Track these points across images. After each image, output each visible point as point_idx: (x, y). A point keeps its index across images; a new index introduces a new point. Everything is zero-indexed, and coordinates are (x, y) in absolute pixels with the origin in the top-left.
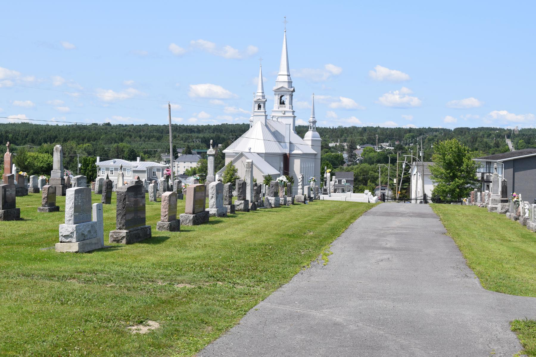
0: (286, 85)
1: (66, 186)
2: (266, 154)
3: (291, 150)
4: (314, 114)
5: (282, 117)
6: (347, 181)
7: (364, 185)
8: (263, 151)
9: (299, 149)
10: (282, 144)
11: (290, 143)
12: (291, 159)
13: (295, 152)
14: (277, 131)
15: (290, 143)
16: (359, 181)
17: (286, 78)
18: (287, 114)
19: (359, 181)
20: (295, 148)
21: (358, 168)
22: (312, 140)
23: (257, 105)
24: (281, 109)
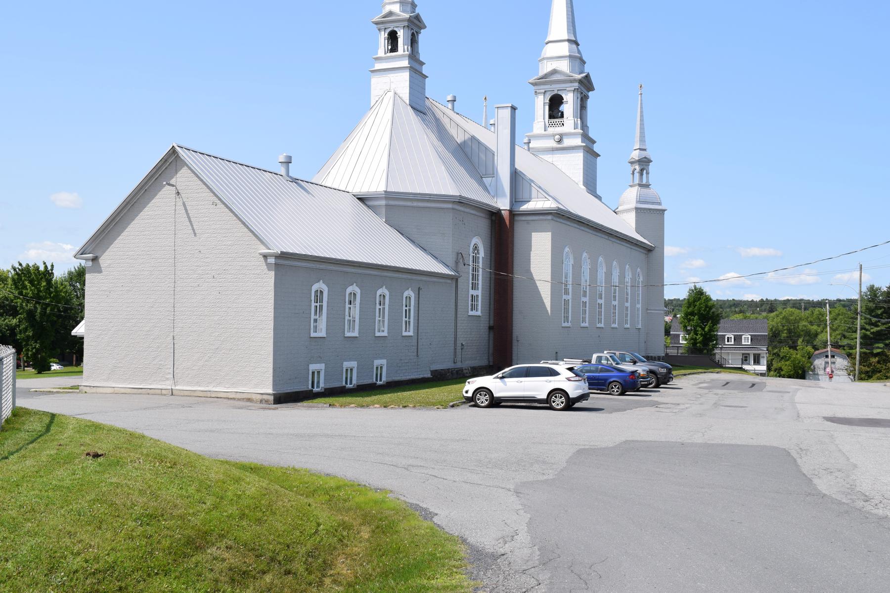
0: (564, 66)
1: (20, 331)
2: (389, 195)
3: (515, 199)
4: (642, 139)
5: (553, 150)
6: (753, 338)
7: (790, 347)
8: (376, 185)
9: (548, 195)
10: (487, 181)
11: (515, 175)
12: (520, 229)
13: (535, 204)
14: (473, 138)
15: (515, 175)
16: (781, 342)
17: (564, 49)
18: (567, 142)
19: (781, 342)
20: (534, 193)
21: (777, 316)
22: (637, 209)
23: (384, 35)
24: (551, 130)
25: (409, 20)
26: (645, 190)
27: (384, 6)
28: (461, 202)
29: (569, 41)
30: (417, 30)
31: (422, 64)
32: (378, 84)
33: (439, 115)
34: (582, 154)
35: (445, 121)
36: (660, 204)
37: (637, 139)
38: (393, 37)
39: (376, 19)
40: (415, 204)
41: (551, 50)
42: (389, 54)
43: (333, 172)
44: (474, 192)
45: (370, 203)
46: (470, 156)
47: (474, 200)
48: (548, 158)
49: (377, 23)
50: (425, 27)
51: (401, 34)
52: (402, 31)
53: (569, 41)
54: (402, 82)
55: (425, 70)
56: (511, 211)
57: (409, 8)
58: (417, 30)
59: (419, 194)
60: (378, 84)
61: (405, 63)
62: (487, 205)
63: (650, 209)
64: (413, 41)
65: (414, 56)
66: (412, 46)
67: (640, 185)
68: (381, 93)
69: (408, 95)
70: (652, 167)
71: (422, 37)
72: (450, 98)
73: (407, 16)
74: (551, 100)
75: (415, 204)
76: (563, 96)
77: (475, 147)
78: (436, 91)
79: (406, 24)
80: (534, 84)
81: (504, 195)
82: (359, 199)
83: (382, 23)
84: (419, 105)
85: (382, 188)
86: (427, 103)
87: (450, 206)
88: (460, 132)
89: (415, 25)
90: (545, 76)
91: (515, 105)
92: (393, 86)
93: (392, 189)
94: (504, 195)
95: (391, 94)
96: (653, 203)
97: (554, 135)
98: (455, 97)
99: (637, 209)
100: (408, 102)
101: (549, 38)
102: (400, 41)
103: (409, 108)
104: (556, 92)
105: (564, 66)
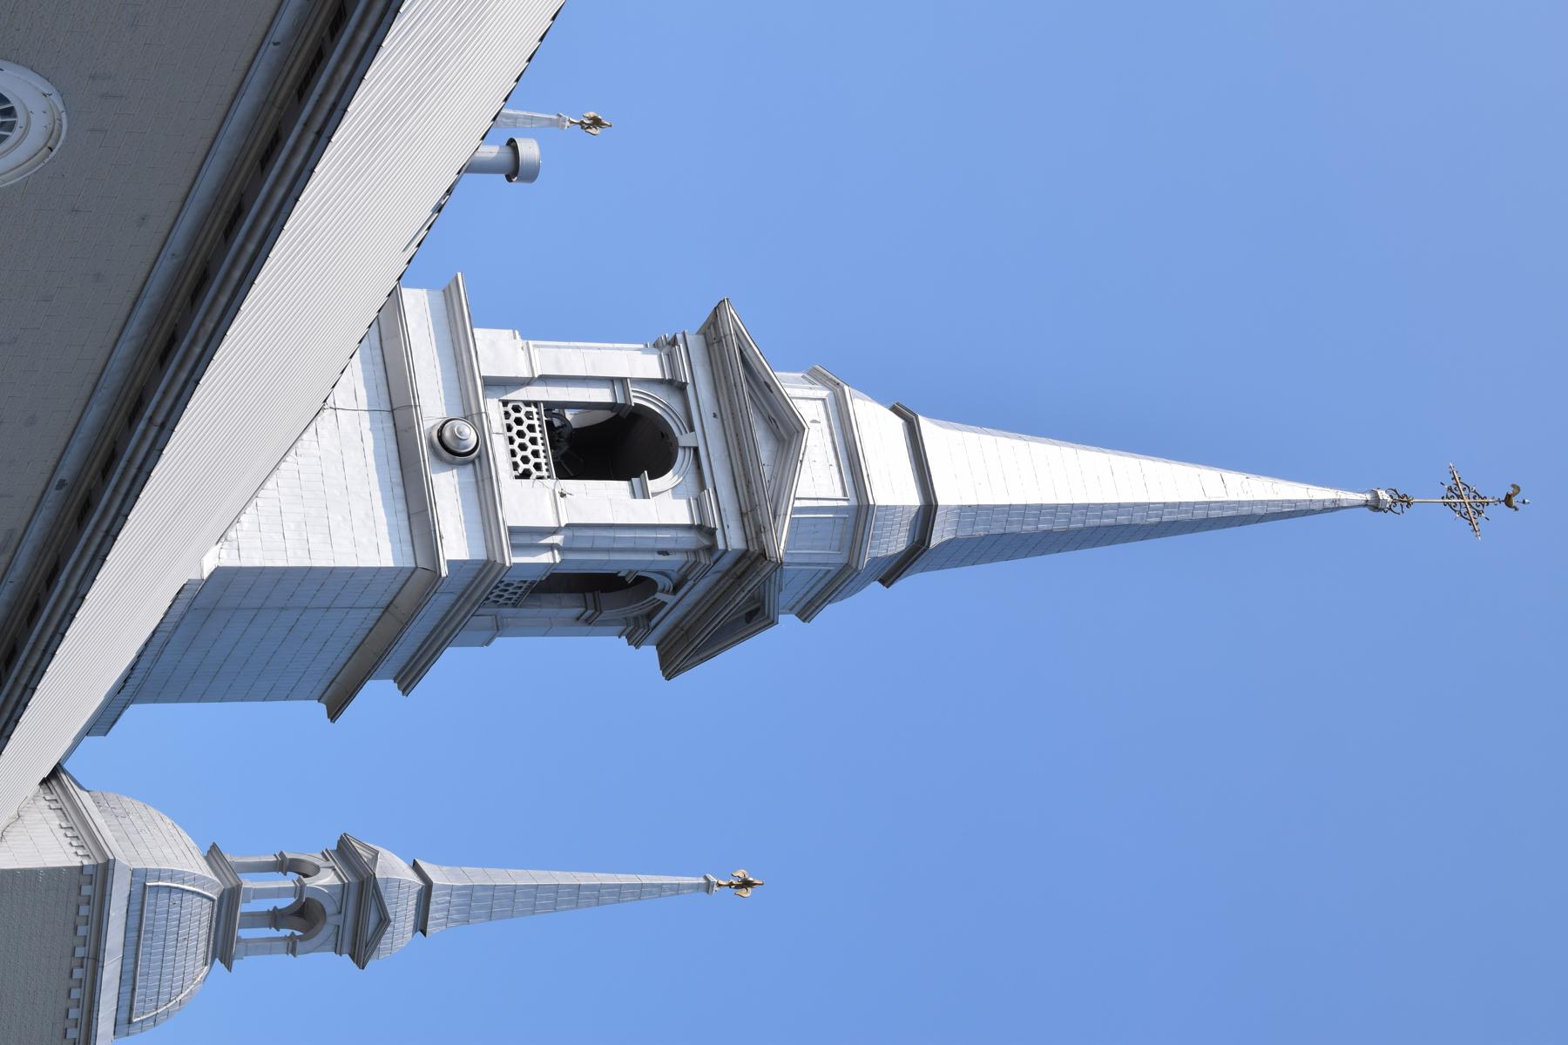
4: (482, 904)
25: (754, 560)
26: (198, 922)
27: (816, 376)
29: (928, 511)
31: (407, 679)
34: (386, 559)
36: (125, 1022)
37: (478, 876)
38: (607, 443)
41: (878, 429)
48: (355, 389)
51: (662, 504)
53: (928, 511)
55: (378, 692)
61: (456, 543)
63: (95, 961)
64: (595, 590)
67: (229, 900)
70: (324, 966)
71: (613, 661)
72: (529, 150)
73: (781, 543)
74: (637, 416)
76: (669, 480)
79: (733, 539)
80: (713, 332)
90: (764, 391)
96: (129, 979)
97: (473, 416)
98: (532, 175)
99: (103, 871)
101: (927, 426)
102: (603, 501)
104: (684, 439)
105: (817, 480)
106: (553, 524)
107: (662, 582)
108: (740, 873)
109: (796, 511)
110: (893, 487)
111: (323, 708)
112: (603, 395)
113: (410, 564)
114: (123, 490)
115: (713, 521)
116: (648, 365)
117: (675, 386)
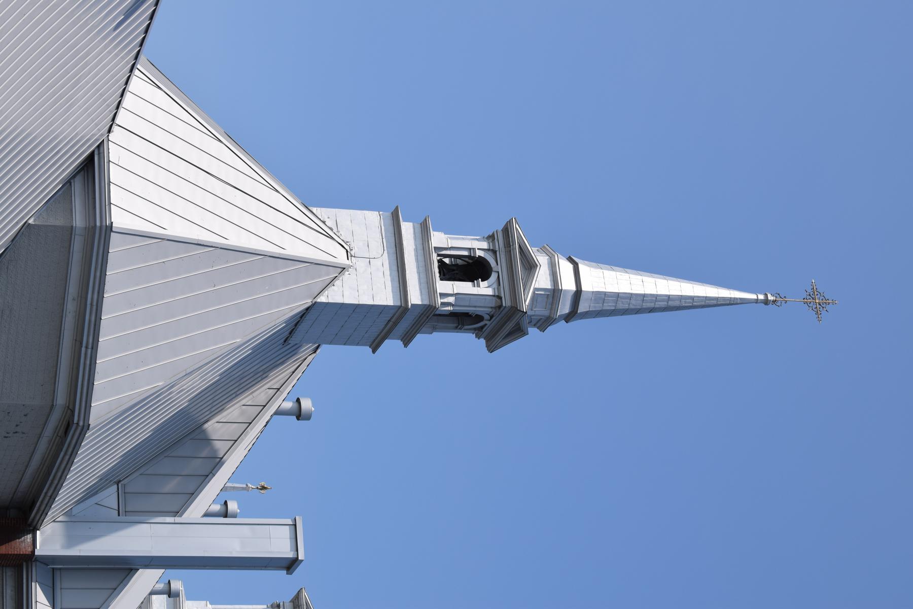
2: (99, 235)
3: (57, 570)
8: (131, 203)
10: (109, 497)
11: (122, 569)
15: (122, 569)
23: (478, 246)
25: (515, 310)
27: (543, 250)
28: (70, 428)
29: (578, 293)
30: (487, 330)
31: (407, 340)
32: (365, 227)
33: (276, 378)
34: (390, 302)
35: (260, 393)
38: (470, 268)
39: (518, 230)
40: (71, 307)
42: (435, 258)
43: (160, 97)
44: (90, 463)
45: (78, 186)
46: (176, 454)
47: (70, 462)
49: (507, 231)
50: (491, 348)
51: (484, 288)
52: (490, 292)
53: (578, 293)
54: (368, 285)
55: (392, 345)
56: (30, 558)
57: (541, 311)
58: (487, 330)
59: (98, 319)
60: (365, 227)
61: (415, 297)
62: (52, 499)
64: (462, 319)
65: (431, 318)
66: (452, 314)
68: (345, 235)
69: (338, 299)
71: (467, 342)
72: (307, 404)
73: (526, 303)
75: (71, 307)
76: (485, 283)
77: (196, 466)
78: (328, 366)
79: (507, 302)
81: (71, 540)
82: (90, 159)
83: (508, 244)
84: (316, 326)
85: (119, 219)
86: (308, 347)
87: (61, 399)
88: (232, 430)
89: (500, 325)
91: (299, 571)
92: (360, 264)
93: (116, 246)
94: (71, 540)
95: (341, 258)
98: (308, 417)
100: (322, 299)
102: (465, 287)
103: (308, 302)
105: (542, 280)
106: (451, 292)
107: (487, 317)
108: (263, 483)
109: (536, 289)
110: (568, 284)
111: (371, 350)
112: (466, 253)
113: (398, 304)
114: (69, 453)
115: (502, 295)
116: (485, 245)
117: (494, 252)
